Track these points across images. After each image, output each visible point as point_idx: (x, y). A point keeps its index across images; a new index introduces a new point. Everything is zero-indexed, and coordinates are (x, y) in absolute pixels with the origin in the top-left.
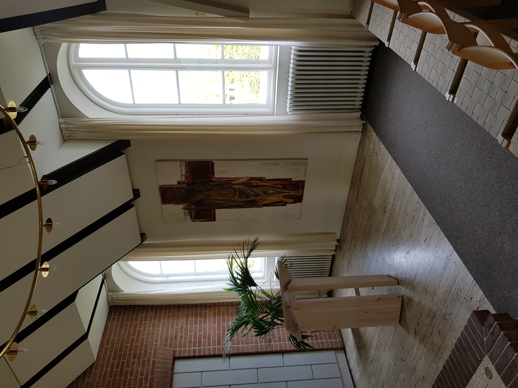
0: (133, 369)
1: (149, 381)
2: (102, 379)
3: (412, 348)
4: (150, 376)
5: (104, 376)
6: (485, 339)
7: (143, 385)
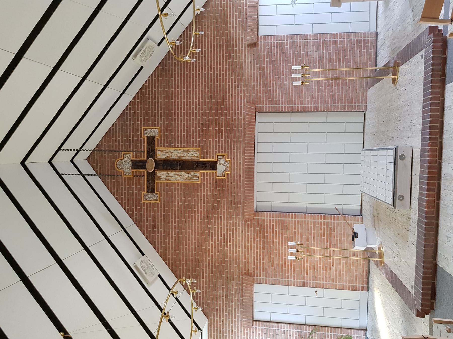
0: (234, 2)
1: (244, 11)
2: (216, 9)
3: (409, 16)
4: (244, 7)
5: (217, 7)
6: (427, 42)
7: (241, 13)
